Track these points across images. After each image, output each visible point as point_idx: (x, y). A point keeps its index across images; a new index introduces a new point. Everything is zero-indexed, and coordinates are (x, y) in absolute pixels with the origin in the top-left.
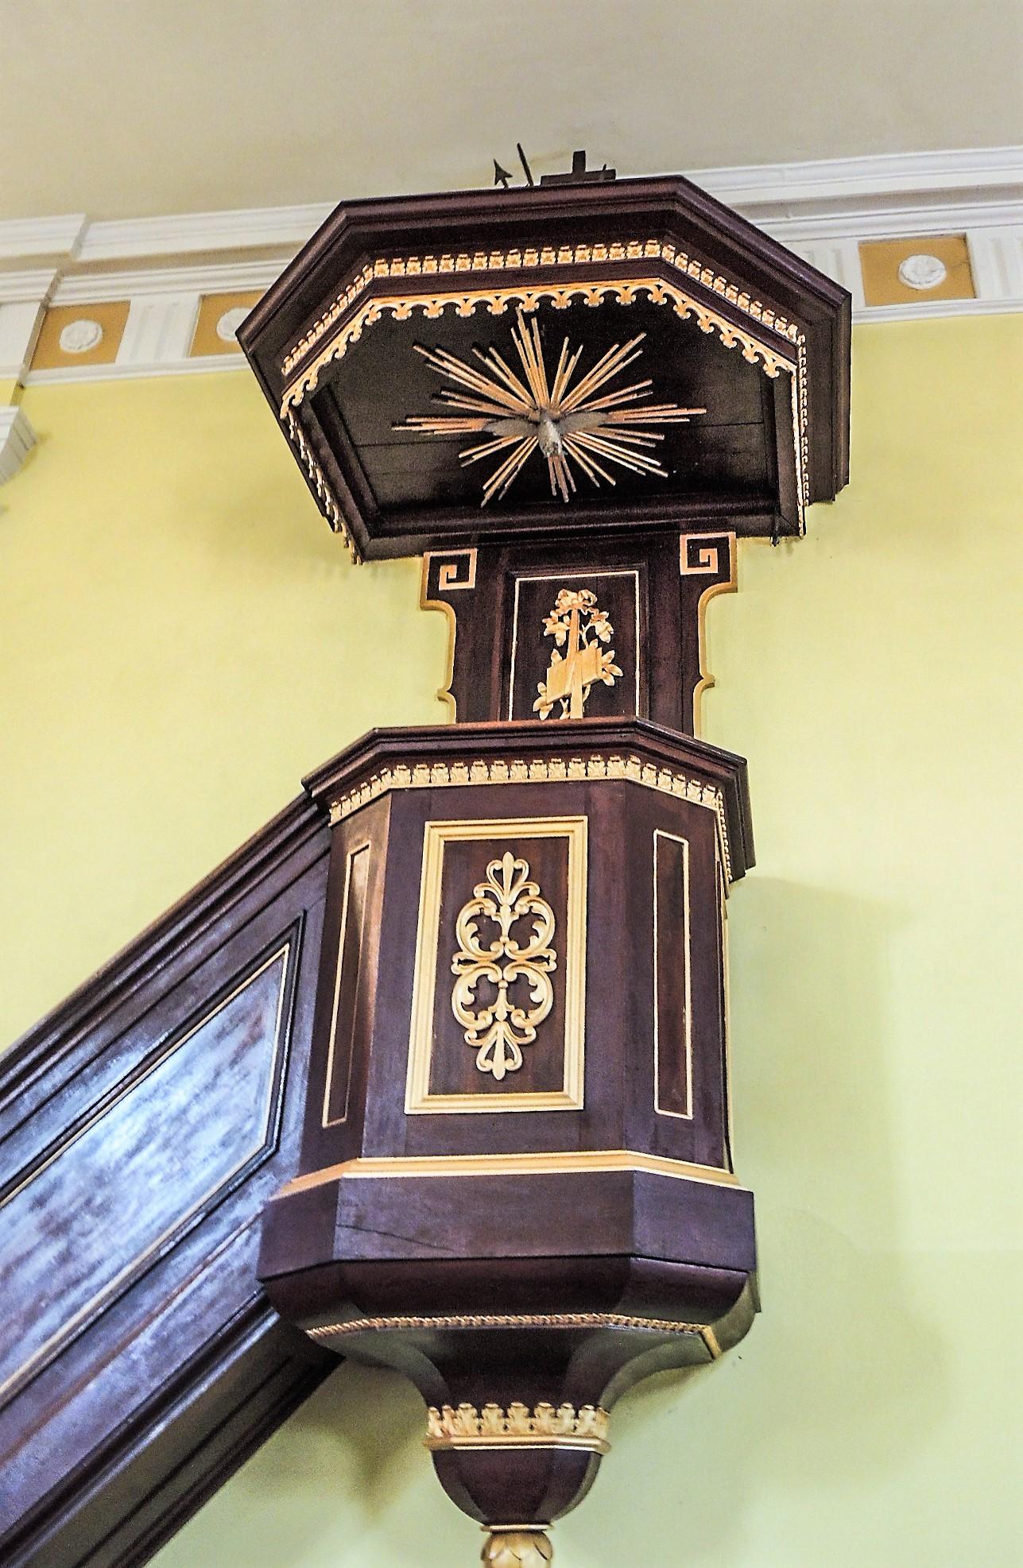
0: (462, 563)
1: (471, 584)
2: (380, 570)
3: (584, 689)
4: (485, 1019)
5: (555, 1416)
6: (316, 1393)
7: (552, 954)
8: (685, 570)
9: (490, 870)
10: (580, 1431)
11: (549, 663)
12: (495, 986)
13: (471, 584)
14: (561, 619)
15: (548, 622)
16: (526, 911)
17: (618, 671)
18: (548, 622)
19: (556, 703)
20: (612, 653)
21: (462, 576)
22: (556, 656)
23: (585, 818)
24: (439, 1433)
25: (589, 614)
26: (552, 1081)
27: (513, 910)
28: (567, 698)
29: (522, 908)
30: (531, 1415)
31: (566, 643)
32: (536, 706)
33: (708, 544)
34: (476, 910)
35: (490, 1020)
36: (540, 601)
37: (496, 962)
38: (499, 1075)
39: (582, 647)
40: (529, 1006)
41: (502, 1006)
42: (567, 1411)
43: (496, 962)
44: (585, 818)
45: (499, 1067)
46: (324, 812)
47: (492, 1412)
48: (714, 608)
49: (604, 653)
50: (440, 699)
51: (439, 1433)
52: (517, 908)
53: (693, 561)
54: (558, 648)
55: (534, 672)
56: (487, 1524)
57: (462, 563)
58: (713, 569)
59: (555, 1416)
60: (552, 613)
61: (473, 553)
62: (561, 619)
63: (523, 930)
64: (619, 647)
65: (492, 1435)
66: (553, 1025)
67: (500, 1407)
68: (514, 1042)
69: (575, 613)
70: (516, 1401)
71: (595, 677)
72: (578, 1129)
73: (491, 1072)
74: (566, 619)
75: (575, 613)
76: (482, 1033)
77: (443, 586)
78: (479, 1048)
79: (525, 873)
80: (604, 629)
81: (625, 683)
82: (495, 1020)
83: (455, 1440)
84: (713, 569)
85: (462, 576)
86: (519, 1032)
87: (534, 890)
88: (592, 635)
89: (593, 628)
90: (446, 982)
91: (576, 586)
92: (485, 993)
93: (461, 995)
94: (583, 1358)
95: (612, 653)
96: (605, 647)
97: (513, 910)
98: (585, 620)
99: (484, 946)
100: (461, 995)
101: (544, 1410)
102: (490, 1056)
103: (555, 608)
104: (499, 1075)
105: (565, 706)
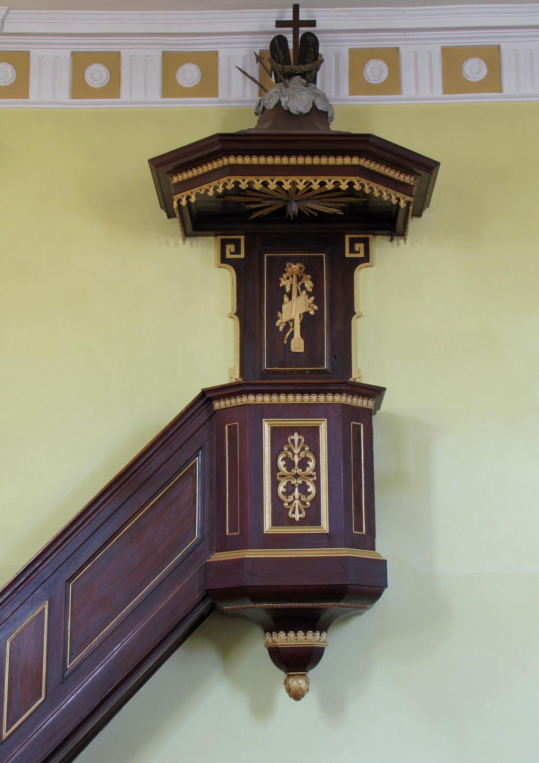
0: (237, 243)
1: (242, 256)
2: (194, 243)
3: (300, 316)
4: (291, 498)
5: (314, 635)
6: (200, 626)
7: (314, 474)
8: (348, 255)
9: (289, 440)
10: (322, 640)
11: (282, 302)
12: (294, 486)
13: (242, 256)
14: (288, 278)
15: (282, 279)
16: (304, 456)
17: (316, 307)
18: (282, 279)
19: (287, 323)
20: (313, 298)
21: (237, 251)
22: (286, 299)
23: (326, 419)
24: (270, 641)
25: (302, 277)
26: (317, 522)
27: (299, 456)
28: (292, 321)
29: (302, 455)
30: (296, 635)
31: (291, 290)
32: (277, 324)
33: (359, 241)
34: (284, 455)
35: (292, 498)
36: (277, 270)
37: (294, 476)
38: (297, 519)
39: (298, 295)
40: (308, 494)
41: (297, 493)
42: (318, 634)
43: (294, 476)
44: (326, 419)
45: (297, 516)
46: (210, 400)
47: (301, 633)
48: (363, 277)
49: (309, 298)
50: (230, 317)
51: (270, 641)
52: (301, 455)
53: (352, 250)
54: (287, 294)
55: (276, 307)
56: (286, 672)
57: (237, 243)
58: (362, 255)
59: (314, 635)
60: (283, 275)
61: (242, 238)
62: (288, 278)
63: (303, 464)
64: (316, 294)
65: (291, 642)
66: (317, 500)
67: (294, 632)
68: (302, 507)
69: (294, 276)
70: (300, 630)
71: (305, 310)
72: (327, 540)
73: (294, 518)
74: (290, 278)
75: (294, 276)
76: (290, 503)
77: (228, 256)
78: (289, 509)
79: (303, 440)
80: (309, 285)
81: (319, 313)
82: (294, 499)
83: (278, 644)
84: (362, 255)
85: (237, 251)
86: (304, 503)
87: (307, 448)
88: (303, 287)
89: (303, 284)
90: (275, 484)
91: (295, 261)
92: (290, 488)
93: (281, 489)
94: (325, 616)
95: (313, 298)
96: (309, 294)
97: (299, 456)
98: (299, 279)
99: (289, 470)
100: (281, 489)
101: (310, 634)
102: (294, 512)
103: (285, 272)
104: (297, 519)
105: (291, 325)
